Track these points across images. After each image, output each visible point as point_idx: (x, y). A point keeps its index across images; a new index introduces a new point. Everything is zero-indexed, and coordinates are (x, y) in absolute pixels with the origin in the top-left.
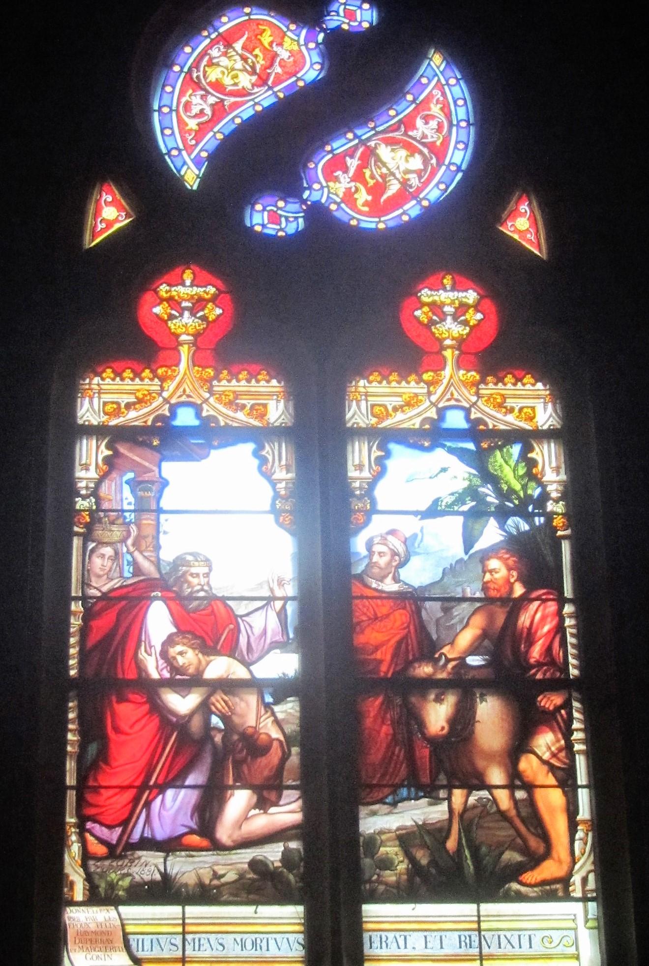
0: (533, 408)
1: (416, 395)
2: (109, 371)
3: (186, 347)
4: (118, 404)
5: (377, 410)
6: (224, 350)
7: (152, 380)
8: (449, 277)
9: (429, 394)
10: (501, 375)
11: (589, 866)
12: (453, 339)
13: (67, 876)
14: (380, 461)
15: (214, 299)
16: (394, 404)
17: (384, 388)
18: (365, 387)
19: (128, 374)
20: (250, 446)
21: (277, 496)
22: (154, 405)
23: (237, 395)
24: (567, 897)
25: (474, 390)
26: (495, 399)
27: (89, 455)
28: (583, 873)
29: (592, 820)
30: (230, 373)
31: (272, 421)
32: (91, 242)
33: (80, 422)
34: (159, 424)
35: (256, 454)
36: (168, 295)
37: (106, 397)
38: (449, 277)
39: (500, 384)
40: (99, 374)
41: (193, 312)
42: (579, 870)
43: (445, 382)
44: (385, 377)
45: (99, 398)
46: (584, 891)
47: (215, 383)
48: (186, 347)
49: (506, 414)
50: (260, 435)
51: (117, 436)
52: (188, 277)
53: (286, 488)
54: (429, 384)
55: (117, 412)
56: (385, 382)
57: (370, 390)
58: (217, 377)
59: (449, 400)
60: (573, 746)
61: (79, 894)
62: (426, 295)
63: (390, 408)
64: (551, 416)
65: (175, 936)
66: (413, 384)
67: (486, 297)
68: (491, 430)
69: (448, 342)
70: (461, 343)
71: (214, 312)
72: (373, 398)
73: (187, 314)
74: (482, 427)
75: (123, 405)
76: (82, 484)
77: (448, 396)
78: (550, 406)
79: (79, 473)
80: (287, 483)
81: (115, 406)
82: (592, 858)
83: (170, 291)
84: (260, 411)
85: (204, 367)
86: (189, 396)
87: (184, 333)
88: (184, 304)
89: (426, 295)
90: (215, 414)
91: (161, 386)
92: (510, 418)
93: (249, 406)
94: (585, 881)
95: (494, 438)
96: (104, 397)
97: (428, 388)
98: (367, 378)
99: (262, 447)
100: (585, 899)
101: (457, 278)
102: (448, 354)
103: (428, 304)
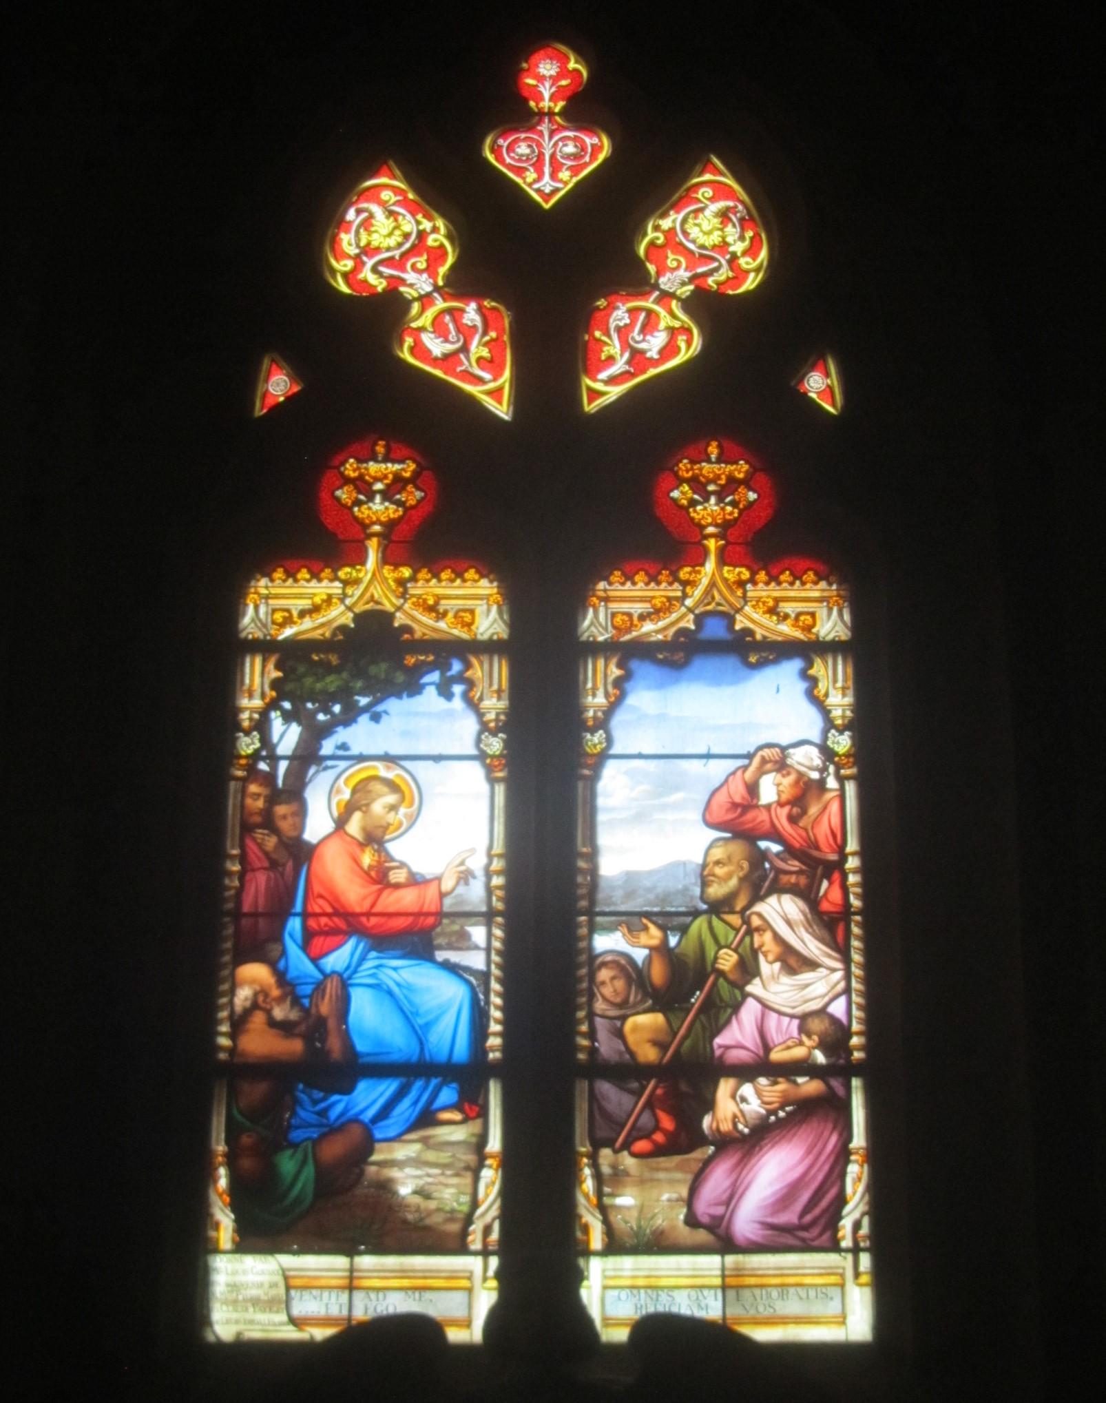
0: (813, 615)
1: (669, 599)
2: (617, 573)
3: (375, 540)
4: (630, 615)
5: (618, 619)
6: (424, 545)
7: (671, 584)
8: (714, 444)
9: (685, 596)
10: (774, 572)
11: (863, 1207)
12: (716, 525)
13: (580, 1217)
14: (619, 683)
15: (414, 479)
16: (640, 611)
17: (289, 588)
18: (267, 587)
19: (786, 576)
20: (796, 665)
21: (484, 727)
22: (674, 616)
23: (438, 598)
24: (461, 1248)
25: (739, 593)
26: (425, 600)
27: (257, 675)
28: (856, 1215)
29: (867, 1149)
30: (624, 574)
31: (481, 630)
32: (259, 411)
33: (584, 638)
34: (682, 639)
35: (804, 674)
36: (690, 473)
37: (614, 606)
38: (714, 444)
39: (629, 584)
40: (269, 575)
41: (387, 495)
42: (483, 1214)
43: (705, 582)
44: (459, 574)
45: (607, 608)
46: (485, 1244)
47: (749, 586)
48: (375, 540)
49: (779, 622)
50: (807, 650)
51: (294, 657)
52: (713, 450)
53: (843, 717)
54: (346, 583)
55: (288, 621)
56: (798, 583)
57: (611, 594)
58: (413, 579)
59: (367, 603)
60: (852, 1054)
61: (596, 1240)
62: (350, 468)
63: (295, 613)
64: (495, 621)
65: (706, 1292)
66: (641, 585)
67: (761, 470)
68: (759, 642)
69: (711, 530)
70: (726, 527)
71: (413, 496)
72: (622, 604)
73: (713, 500)
74: (406, 636)
75: (295, 613)
76: (245, 716)
77: (368, 595)
78: (494, 608)
79: (244, 702)
80: (844, 711)
81: (286, 614)
82: (867, 1198)
83: (692, 469)
84: (465, 618)
85: (397, 566)
86: (719, 604)
87: (711, 525)
88: (377, 486)
89: (350, 468)
90: (409, 622)
91: (684, 592)
92: (442, 625)
93: (793, 615)
94: (487, 1230)
95: (764, 651)
96: (289, 604)
97: (344, 589)
98: (606, 578)
99: (810, 664)
100: (485, 1253)
101: (726, 444)
102: (712, 544)
103: (688, 481)
